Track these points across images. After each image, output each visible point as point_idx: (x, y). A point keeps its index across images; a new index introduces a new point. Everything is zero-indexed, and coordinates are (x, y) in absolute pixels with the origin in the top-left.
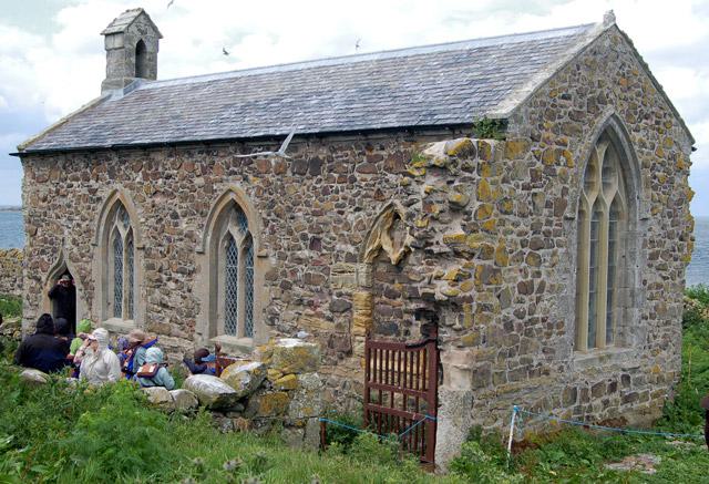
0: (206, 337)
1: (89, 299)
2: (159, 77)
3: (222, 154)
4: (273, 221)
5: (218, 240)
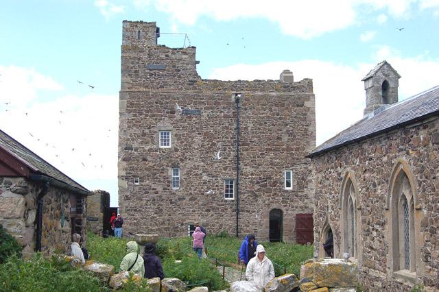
0: (392, 270)
1: (339, 244)
2: (399, 101)
3: (394, 138)
4: (424, 181)
5: (397, 200)
